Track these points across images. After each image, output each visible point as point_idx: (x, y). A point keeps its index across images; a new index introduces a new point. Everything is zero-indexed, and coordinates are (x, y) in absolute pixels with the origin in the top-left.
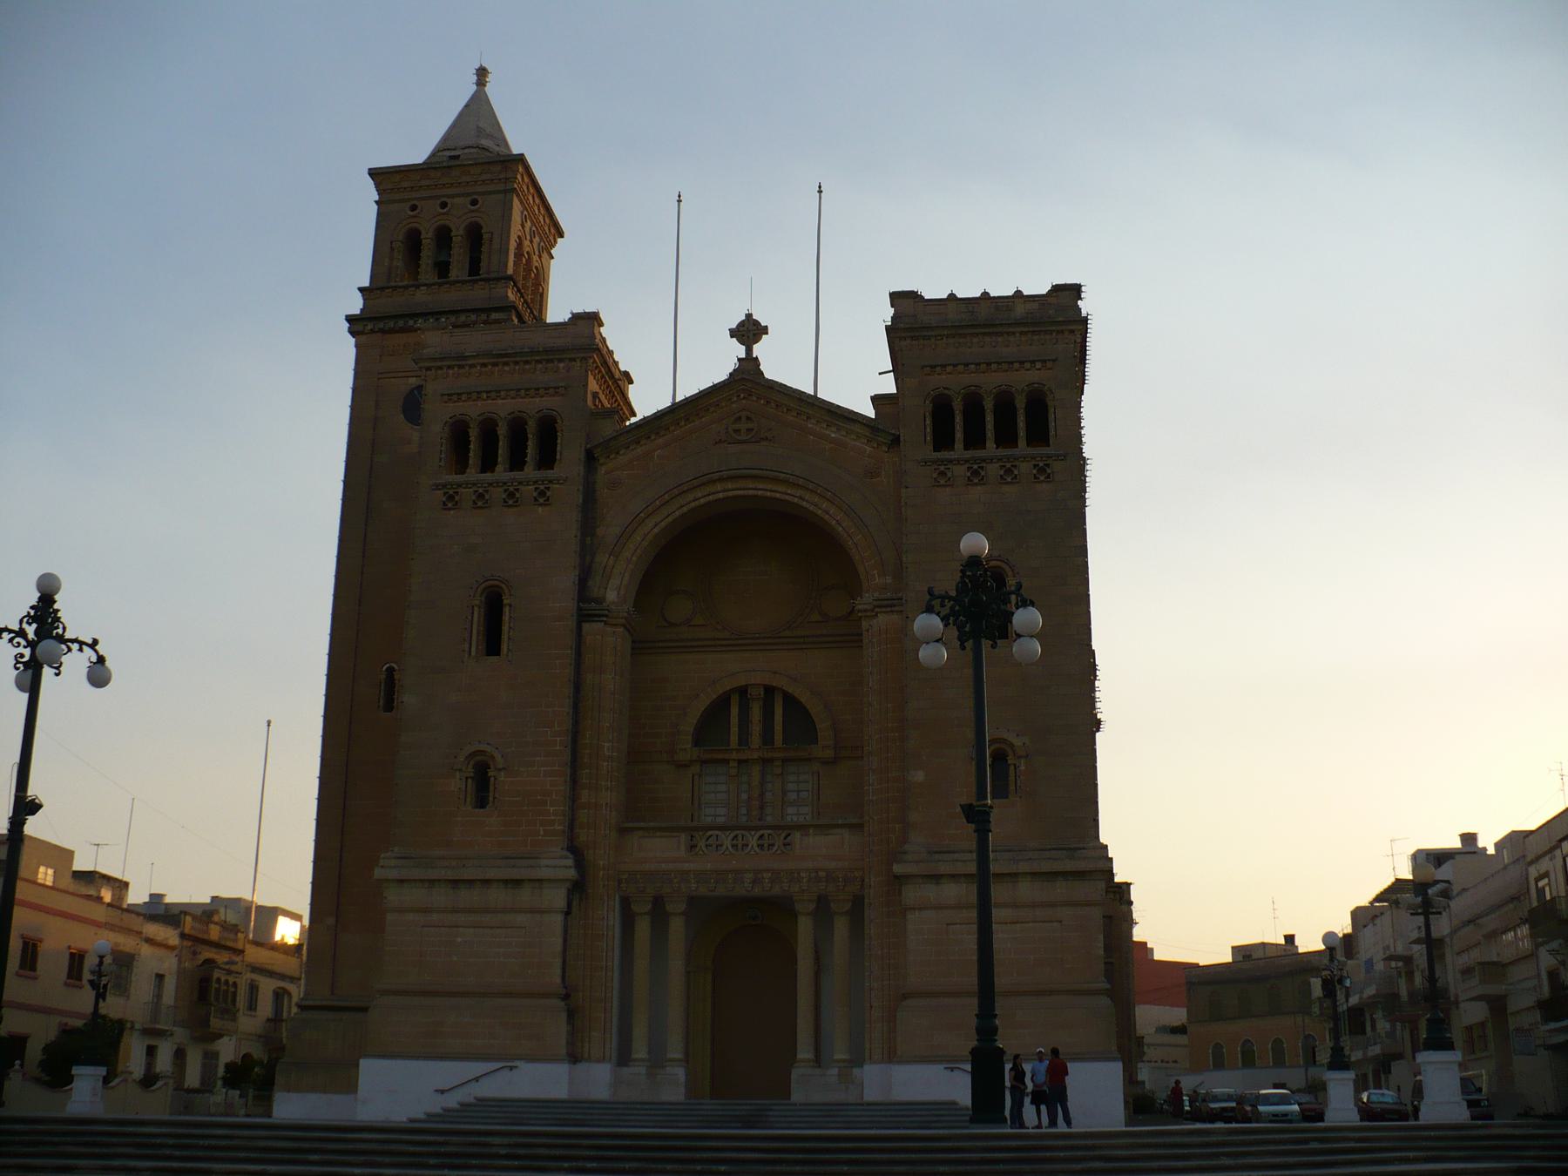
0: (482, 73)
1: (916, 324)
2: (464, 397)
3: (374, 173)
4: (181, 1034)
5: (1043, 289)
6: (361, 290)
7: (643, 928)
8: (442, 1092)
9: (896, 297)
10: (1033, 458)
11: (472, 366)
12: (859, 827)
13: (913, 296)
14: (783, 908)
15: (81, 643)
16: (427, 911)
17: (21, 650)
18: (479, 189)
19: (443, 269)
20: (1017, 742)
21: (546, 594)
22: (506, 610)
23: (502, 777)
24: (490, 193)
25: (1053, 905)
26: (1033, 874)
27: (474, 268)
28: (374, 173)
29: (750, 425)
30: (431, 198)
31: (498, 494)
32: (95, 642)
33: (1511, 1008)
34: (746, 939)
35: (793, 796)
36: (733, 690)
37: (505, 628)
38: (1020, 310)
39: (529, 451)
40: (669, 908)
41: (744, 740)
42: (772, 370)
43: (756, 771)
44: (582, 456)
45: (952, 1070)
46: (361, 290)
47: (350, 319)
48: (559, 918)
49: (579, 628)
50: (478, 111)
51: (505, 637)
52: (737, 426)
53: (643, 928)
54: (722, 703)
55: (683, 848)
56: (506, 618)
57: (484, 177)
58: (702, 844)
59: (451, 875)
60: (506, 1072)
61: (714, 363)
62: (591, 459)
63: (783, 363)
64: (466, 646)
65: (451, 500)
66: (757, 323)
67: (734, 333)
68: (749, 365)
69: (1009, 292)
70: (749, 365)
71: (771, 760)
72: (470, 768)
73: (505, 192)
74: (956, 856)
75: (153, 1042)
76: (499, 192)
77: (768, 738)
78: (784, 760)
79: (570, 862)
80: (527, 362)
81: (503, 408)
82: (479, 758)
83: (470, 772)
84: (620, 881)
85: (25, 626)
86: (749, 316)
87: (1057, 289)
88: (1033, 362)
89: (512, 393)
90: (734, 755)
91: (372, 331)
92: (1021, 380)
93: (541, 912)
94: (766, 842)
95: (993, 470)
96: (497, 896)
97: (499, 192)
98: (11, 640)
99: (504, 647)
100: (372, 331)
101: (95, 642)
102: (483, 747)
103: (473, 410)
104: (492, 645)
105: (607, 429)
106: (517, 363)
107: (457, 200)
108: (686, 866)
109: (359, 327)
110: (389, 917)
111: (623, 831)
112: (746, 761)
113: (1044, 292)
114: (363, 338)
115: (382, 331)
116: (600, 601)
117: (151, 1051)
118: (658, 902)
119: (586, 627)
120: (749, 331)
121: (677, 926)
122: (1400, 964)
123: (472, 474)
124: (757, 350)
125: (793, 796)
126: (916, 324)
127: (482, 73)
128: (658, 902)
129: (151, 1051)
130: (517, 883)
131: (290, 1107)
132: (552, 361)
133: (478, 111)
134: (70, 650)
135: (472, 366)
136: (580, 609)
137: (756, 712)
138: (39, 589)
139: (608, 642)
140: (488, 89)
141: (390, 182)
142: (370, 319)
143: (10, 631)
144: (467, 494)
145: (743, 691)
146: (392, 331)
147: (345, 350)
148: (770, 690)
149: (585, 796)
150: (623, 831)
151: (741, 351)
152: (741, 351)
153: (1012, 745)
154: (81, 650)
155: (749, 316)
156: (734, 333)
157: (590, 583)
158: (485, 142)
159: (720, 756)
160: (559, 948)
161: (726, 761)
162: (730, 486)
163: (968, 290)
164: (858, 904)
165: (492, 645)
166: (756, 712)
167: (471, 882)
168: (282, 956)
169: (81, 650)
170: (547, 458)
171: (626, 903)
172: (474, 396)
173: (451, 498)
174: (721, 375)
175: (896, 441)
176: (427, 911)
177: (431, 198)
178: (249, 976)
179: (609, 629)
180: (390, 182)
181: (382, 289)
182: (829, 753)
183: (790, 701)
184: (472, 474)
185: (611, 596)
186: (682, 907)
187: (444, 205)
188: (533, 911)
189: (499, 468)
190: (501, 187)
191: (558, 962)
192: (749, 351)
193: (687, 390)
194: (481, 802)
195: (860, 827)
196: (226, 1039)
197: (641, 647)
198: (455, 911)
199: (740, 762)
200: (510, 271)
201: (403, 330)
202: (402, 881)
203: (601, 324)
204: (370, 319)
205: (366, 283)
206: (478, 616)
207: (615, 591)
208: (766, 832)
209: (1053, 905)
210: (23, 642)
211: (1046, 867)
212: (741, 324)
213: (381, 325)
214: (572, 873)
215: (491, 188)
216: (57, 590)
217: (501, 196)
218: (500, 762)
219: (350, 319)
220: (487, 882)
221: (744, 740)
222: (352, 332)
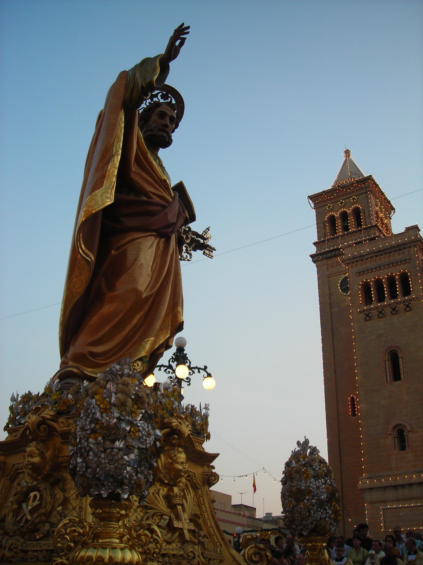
0: (347, 152)
2: (366, 272)
3: (311, 198)
6: (315, 244)
11: (366, 259)
15: (199, 369)
17: (170, 375)
19: (346, 228)
22: (400, 360)
23: (411, 435)
27: (359, 224)
28: (311, 198)
31: (388, 310)
32: (206, 367)
37: (401, 368)
46: (315, 244)
47: (312, 256)
50: (349, 165)
51: (402, 372)
56: (401, 363)
64: (385, 378)
65: (368, 316)
72: (395, 433)
76: (363, 193)
80: (390, 252)
81: (383, 276)
82: (399, 427)
83: (395, 434)
85: (171, 363)
87: (408, 229)
89: (386, 266)
91: (322, 259)
98: (165, 371)
99: (402, 376)
100: (322, 259)
101: (206, 367)
102: (400, 422)
103: (371, 279)
104: (397, 376)
106: (386, 254)
109: (316, 258)
114: (319, 263)
115: (326, 258)
127: (347, 152)
132: (400, 250)
133: (349, 165)
134: (194, 372)
135: (366, 259)
140: (352, 157)
141: (319, 200)
143: (165, 366)
146: (330, 257)
147: (312, 269)
154: (199, 372)
165: (397, 376)
168: (134, 237)
169: (199, 372)
172: (370, 271)
173: (368, 315)
180: (319, 200)
181: (323, 241)
189: (386, 299)
194: (403, 448)
203: (419, 230)
205: (316, 240)
206: (388, 364)
210: (171, 371)
213: (325, 256)
215: (360, 192)
216: (185, 344)
217: (365, 195)
218: (409, 428)
219: (312, 256)
222: (314, 262)
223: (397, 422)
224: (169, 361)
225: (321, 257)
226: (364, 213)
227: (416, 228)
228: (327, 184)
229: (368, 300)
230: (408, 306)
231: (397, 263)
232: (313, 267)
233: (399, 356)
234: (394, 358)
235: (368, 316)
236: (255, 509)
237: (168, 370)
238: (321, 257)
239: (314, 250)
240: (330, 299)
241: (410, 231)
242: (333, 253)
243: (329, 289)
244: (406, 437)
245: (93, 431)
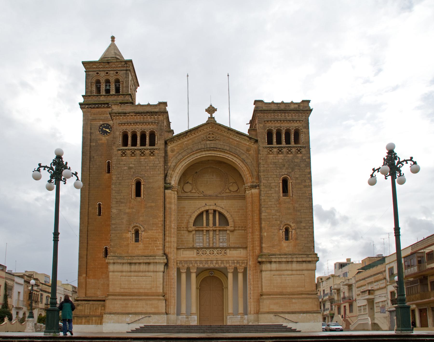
0: (113, 38)
1: (261, 109)
3: (84, 63)
4: (25, 309)
5: (299, 101)
6: (83, 96)
7: (184, 276)
8: (129, 324)
9: (256, 102)
10: (296, 147)
11: (128, 116)
12: (246, 248)
13: (262, 101)
14: (223, 272)
16: (122, 272)
18: (118, 69)
20: (292, 225)
21: (153, 182)
23: (143, 233)
24: (122, 70)
25: (303, 270)
26: (297, 261)
27: (117, 90)
28: (84, 63)
29: (213, 136)
30: (103, 71)
33: (375, 302)
34: (211, 280)
35: (221, 240)
36: (204, 211)
38: (292, 107)
39: (147, 141)
40: (191, 271)
41: (208, 224)
42: (219, 120)
43: (211, 233)
44: (164, 142)
45: (276, 316)
46: (83, 96)
47: (81, 104)
48: (162, 274)
49: (165, 192)
50: (113, 46)
52: (209, 136)
53: (184, 276)
54: (201, 214)
55: (195, 254)
57: (119, 66)
58: (201, 253)
59: (129, 261)
60: (147, 318)
61: (204, 118)
62: (166, 143)
63: (221, 118)
65: (124, 154)
66: (213, 108)
67: (207, 110)
68: (211, 118)
69: (289, 101)
70: (211, 118)
71: (216, 230)
73: (127, 70)
74: (276, 256)
75: (18, 311)
76: (124, 70)
77: (214, 224)
78: (219, 230)
79: (165, 258)
81: (139, 129)
82: (136, 228)
83: (133, 231)
84: (177, 263)
85: (52, 166)
86: (211, 106)
87: (303, 101)
88: (296, 121)
90: (205, 229)
91: (88, 108)
92: (293, 126)
93: (156, 272)
94: (212, 252)
95: (284, 150)
96: (143, 267)
97: (124, 70)
98: (48, 171)
100: (88, 108)
102: (137, 225)
105: (170, 136)
107: (111, 72)
108: (197, 259)
109: (83, 106)
110: (110, 274)
111: (178, 249)
112: (208, 230)
113: (299, 102)
114: (85, 110)
115: (91, 108)
116: (170, 184)
117: (17, 313)
118: (188, 269)
119: (166, 191)
120: (211, 110)
121: (193, 276)
122: (335, 291)
123: (129, 147)
124: (214, 115)
125: (221, 240)
126: (261, 109)
127: (113, 38)
128: (188, 269)
129: (17, 313)
130: (149, 263)
131: (78, 330)
133: (113, 46)
136: (165, 186)
137: (211, 216)
138: (387, 149)
139: (171, 195)
140: (116, 42)
142: (87, 104)
143: (48, 167)
144: (128, 152)
145: (207, 211)
146: (94, 108)
147: (79, 114)
148: (215, 211)
149: (167, 239)
150: (178, 249)
151: (209, 115)
152: (209, 115)
153: (290, 226)
155: (211, 106)
156: (207, 110)
157: (167, 179)
158: (118, 57)
159: (201, 229)
160: (162, 282)
161: (203, 230)
162: (207, 153)
163: (278, 100)
164: (245, 269)
166: (211, 216)
167: (135, 263)
170: (152, 143)
171: (178, 270)
174: (204, 121)
175: (256, 141)
176: (122, 272)
177: (103, 71)
178: (41, 292)
179: (173, 192)
182: (232, 228)
183: (220, 213)
184: (129, 147)
185: (173, 183)
186: (195, 270)
187: (107, 73)
188: (154, 272)
189: (147, 146)
190: (125, 69)
191: (161, 286)
192: (211, 115)
193: (191, 127)
195: (246, 248)
196: (35, 310)
197: (180, 198)
198: (131, 272)
199: (206, 230)
200: (130, 93)
201: (97, 108)
202: (114, 263)
203: (167, 106)
204: (87, 104)
205: (84, 94)
207: (174, 181)
208: (219, 249)
209: (303, 270)
211: (300, 260)
212: (209, 108)
214: (166, 261)
219: (81, 104)
220: (140, 263)
221: (208, 224)
223: (135, 224)
224: (51, 164)
225: (87, 106)
226: (123, 84)
227: (165, 104)
228: (96, 58)
229: (125, 143)
230: (152, 153)
231: (149, 123)
232: (80, 113)
233: (142, 183)
234: (138, 184)
235: (124, 154)
236: (6, 267)
237: (50, 171)
238: (87, 106)
239: (82, 100)
240: (90, 136)
241: (161, 105)
242: (97, 106)
243: (91, 129)
244: (290, 232)
245: (243, 209)
